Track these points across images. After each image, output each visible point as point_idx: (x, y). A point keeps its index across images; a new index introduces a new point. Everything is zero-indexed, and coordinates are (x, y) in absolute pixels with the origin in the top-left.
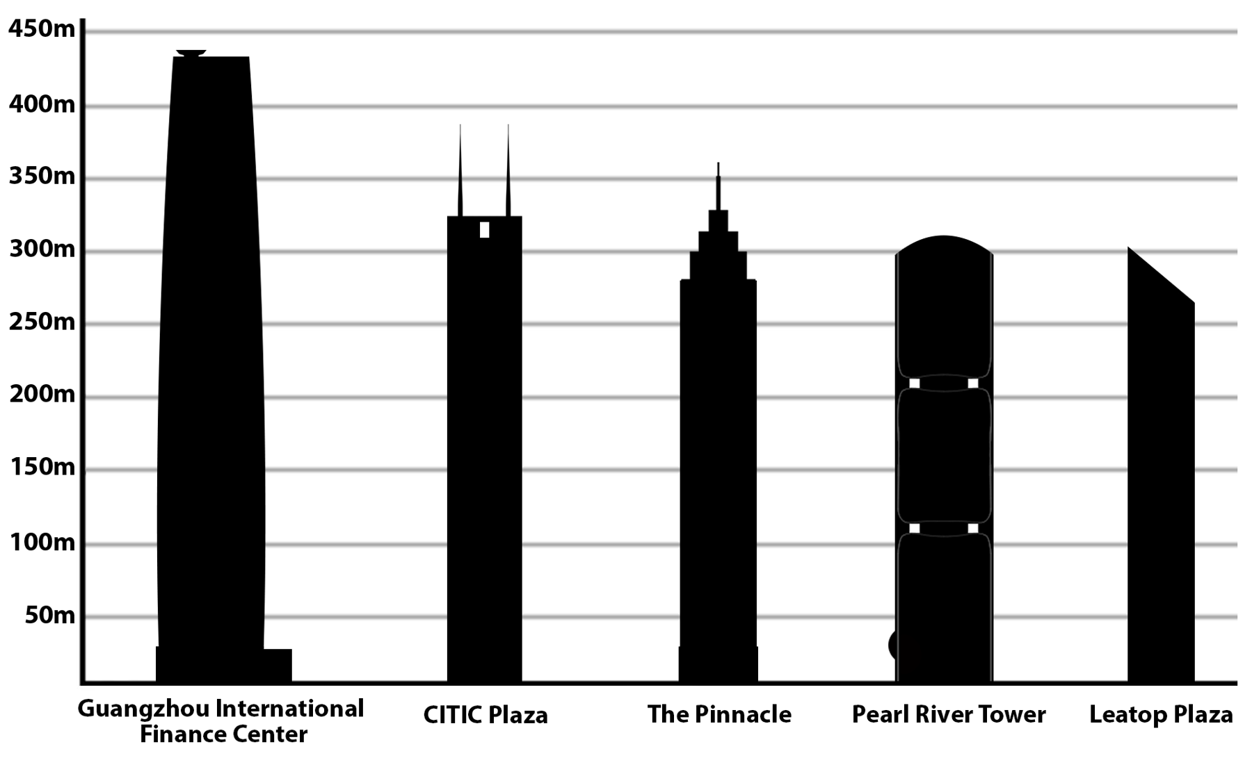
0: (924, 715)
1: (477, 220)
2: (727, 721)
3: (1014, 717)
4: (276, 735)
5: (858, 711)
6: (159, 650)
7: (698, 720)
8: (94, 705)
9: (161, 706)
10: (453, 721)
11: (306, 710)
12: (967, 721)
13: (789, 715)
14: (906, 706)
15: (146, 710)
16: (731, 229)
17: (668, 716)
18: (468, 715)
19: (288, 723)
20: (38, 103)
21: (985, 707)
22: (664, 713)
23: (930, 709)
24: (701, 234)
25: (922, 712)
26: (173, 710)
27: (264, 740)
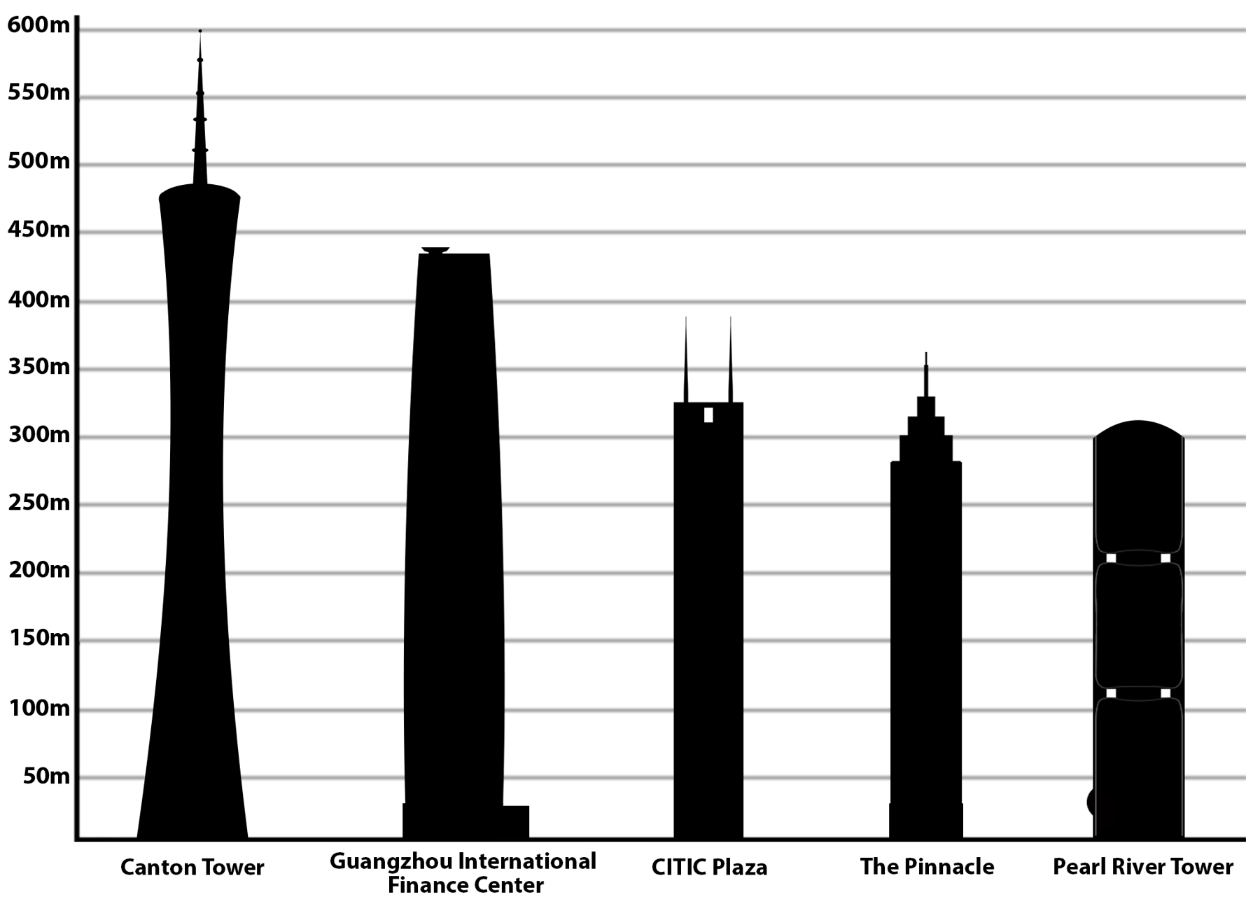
0: (1120, 867)
1: (701, 407)
2: (934, 872)
3: (1203, 869)
4: (515, 886)
5: (1058, 864)
6: (891, 805)
7: (908, 872)
8: (345, 858)
9: (408, 859)
10: (679, 873)
11: (543, 863)
12: (1160, 872)
13: (992, 867)
14: (1103, 859)
15: (393, 863)
16: (938, 414)
17: (879, 868)
18: (693, 867)
19: (526, 875)
20: (36, 299)
21: (1177, 860)
22: (876, 865)
23: (1126, 862)
24: (910, 419)
25: (1118, 865)
26: (419, 862)
27: (504, 891)
